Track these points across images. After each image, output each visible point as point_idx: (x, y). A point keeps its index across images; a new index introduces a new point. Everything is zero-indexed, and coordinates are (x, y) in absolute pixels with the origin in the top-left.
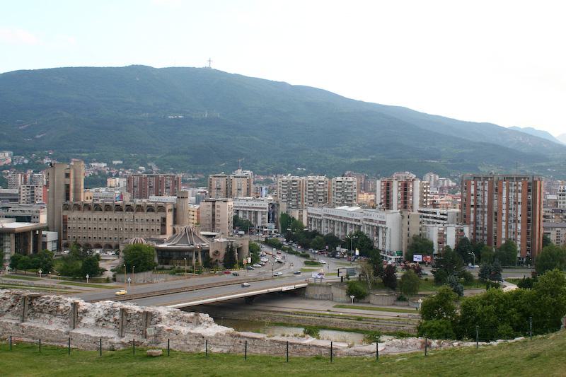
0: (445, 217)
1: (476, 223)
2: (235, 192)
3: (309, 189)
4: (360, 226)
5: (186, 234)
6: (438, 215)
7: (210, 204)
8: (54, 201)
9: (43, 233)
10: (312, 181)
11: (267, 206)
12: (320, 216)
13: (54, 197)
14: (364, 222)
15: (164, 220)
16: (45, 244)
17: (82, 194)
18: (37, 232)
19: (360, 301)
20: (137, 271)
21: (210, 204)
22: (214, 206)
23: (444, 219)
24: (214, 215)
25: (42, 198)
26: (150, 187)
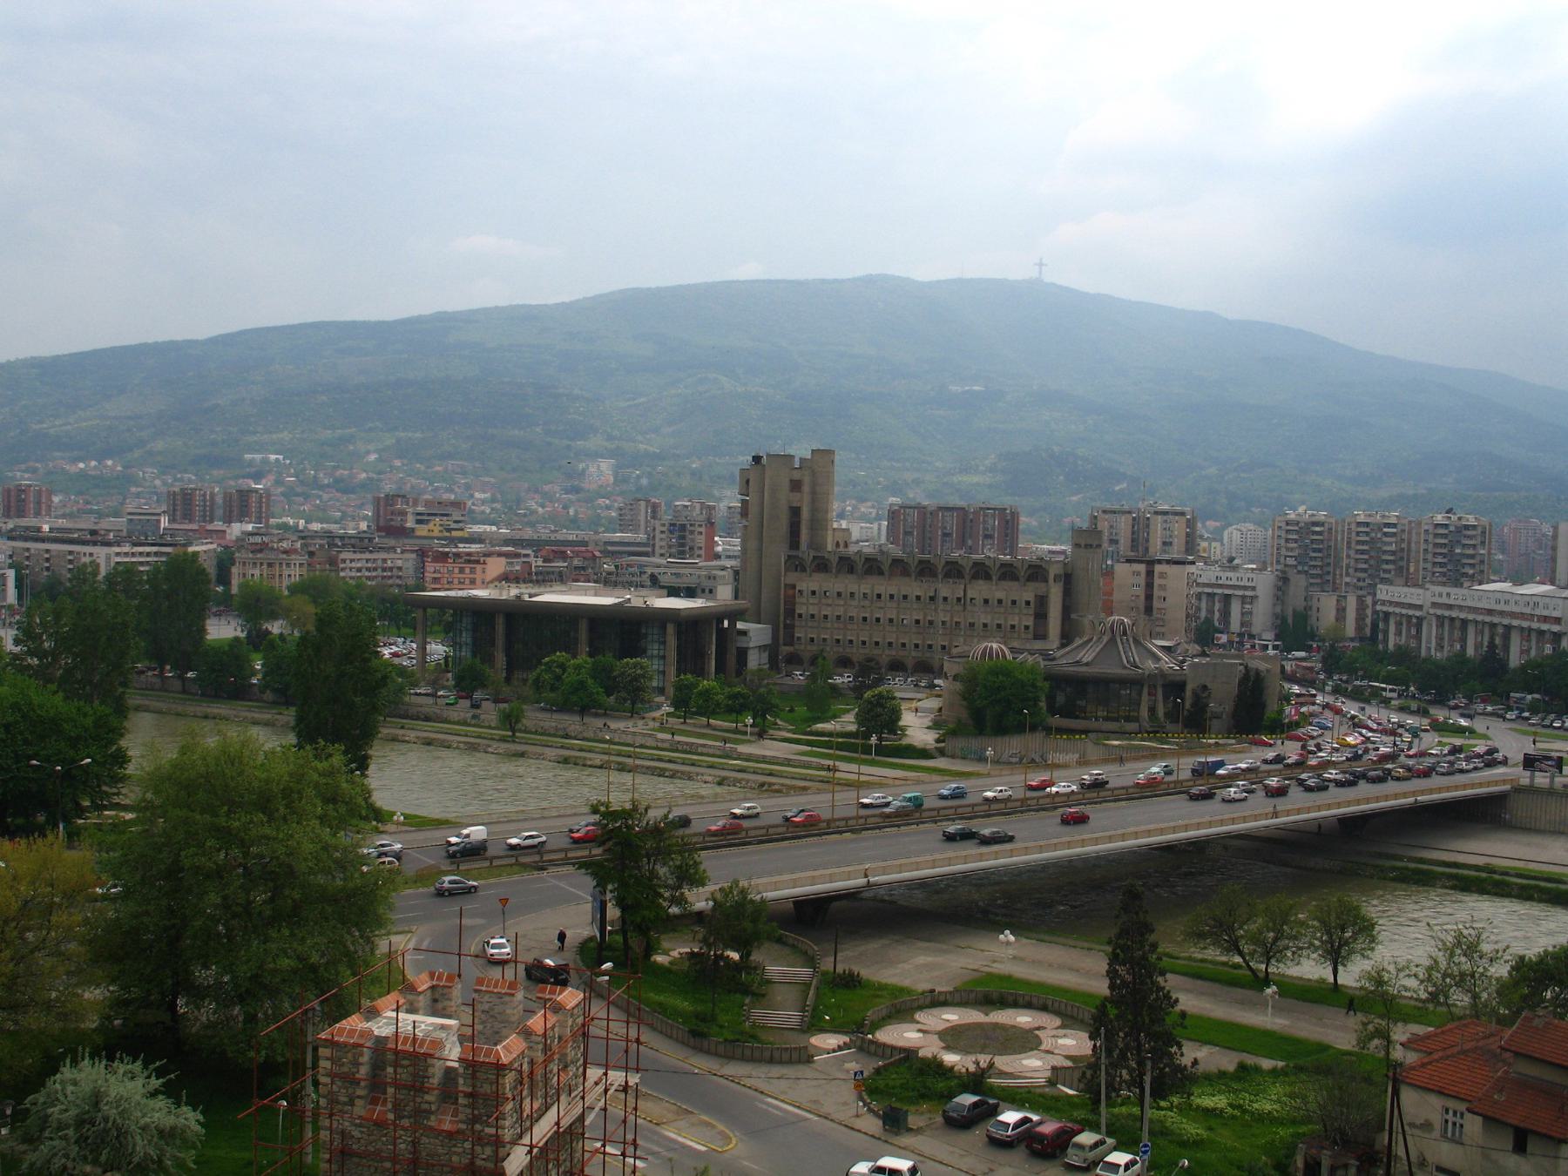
3: (1358, 542)
4: (1557, 637)
7: (1142, 568)
8: (760, 550)
9: (740, 625)
10: (1367, 524)
12: (1420, 607)
13: (761, 539)
14: (1432, 611)
15: (1042, 601)
16: (742, 654)
18: (726, 623)
19: (763, 832)
20: (1001, 730)
21: (1142, 568)
22: (1150, 574)
25: (702, 552)
26: (945, 535)
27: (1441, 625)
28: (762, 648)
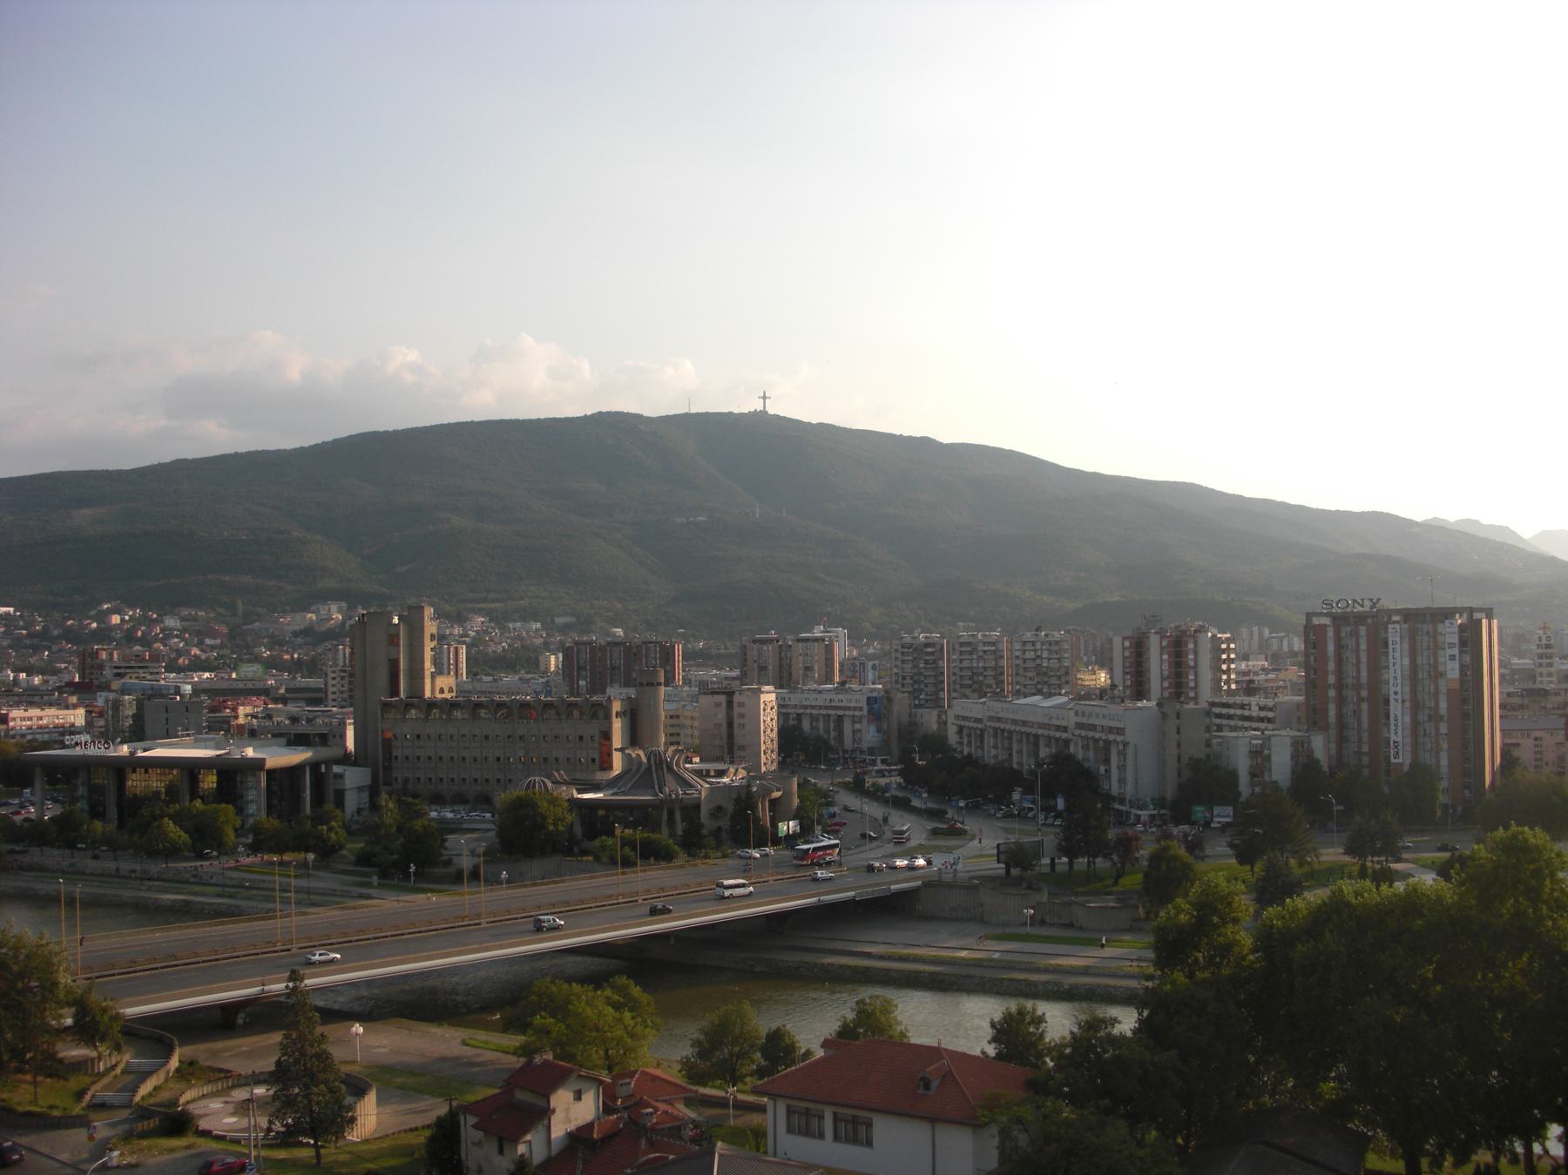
0: (1270, 714)
1: (1341, 725)
2: (798, 671)
4: (1067, 742)
5: (649, 768)
6: (1255, 712)
7: (722, 699)
11: (864, 704)
12: (1065, 729)
16: (340, 795)
17: (428, 681)
18: (323, 768)
21: (722, 699)
22: (730, 704)
23: (1269, 720)
24: (730, 724)
27: (995, 736)
28: (360, 789)
